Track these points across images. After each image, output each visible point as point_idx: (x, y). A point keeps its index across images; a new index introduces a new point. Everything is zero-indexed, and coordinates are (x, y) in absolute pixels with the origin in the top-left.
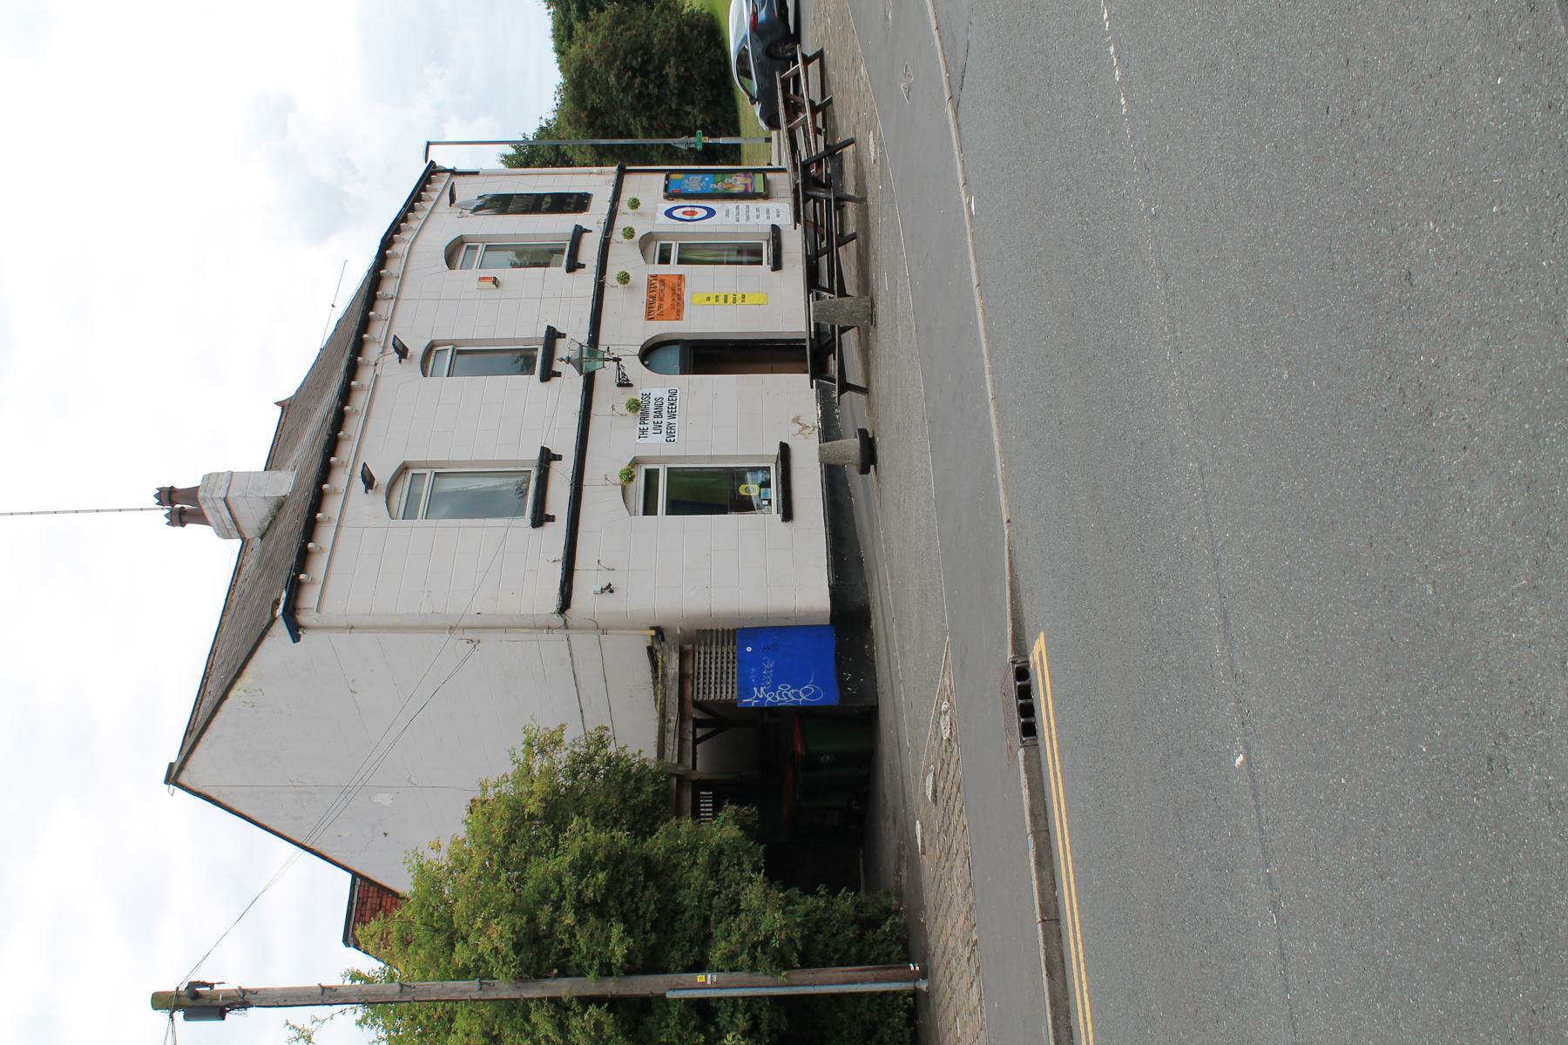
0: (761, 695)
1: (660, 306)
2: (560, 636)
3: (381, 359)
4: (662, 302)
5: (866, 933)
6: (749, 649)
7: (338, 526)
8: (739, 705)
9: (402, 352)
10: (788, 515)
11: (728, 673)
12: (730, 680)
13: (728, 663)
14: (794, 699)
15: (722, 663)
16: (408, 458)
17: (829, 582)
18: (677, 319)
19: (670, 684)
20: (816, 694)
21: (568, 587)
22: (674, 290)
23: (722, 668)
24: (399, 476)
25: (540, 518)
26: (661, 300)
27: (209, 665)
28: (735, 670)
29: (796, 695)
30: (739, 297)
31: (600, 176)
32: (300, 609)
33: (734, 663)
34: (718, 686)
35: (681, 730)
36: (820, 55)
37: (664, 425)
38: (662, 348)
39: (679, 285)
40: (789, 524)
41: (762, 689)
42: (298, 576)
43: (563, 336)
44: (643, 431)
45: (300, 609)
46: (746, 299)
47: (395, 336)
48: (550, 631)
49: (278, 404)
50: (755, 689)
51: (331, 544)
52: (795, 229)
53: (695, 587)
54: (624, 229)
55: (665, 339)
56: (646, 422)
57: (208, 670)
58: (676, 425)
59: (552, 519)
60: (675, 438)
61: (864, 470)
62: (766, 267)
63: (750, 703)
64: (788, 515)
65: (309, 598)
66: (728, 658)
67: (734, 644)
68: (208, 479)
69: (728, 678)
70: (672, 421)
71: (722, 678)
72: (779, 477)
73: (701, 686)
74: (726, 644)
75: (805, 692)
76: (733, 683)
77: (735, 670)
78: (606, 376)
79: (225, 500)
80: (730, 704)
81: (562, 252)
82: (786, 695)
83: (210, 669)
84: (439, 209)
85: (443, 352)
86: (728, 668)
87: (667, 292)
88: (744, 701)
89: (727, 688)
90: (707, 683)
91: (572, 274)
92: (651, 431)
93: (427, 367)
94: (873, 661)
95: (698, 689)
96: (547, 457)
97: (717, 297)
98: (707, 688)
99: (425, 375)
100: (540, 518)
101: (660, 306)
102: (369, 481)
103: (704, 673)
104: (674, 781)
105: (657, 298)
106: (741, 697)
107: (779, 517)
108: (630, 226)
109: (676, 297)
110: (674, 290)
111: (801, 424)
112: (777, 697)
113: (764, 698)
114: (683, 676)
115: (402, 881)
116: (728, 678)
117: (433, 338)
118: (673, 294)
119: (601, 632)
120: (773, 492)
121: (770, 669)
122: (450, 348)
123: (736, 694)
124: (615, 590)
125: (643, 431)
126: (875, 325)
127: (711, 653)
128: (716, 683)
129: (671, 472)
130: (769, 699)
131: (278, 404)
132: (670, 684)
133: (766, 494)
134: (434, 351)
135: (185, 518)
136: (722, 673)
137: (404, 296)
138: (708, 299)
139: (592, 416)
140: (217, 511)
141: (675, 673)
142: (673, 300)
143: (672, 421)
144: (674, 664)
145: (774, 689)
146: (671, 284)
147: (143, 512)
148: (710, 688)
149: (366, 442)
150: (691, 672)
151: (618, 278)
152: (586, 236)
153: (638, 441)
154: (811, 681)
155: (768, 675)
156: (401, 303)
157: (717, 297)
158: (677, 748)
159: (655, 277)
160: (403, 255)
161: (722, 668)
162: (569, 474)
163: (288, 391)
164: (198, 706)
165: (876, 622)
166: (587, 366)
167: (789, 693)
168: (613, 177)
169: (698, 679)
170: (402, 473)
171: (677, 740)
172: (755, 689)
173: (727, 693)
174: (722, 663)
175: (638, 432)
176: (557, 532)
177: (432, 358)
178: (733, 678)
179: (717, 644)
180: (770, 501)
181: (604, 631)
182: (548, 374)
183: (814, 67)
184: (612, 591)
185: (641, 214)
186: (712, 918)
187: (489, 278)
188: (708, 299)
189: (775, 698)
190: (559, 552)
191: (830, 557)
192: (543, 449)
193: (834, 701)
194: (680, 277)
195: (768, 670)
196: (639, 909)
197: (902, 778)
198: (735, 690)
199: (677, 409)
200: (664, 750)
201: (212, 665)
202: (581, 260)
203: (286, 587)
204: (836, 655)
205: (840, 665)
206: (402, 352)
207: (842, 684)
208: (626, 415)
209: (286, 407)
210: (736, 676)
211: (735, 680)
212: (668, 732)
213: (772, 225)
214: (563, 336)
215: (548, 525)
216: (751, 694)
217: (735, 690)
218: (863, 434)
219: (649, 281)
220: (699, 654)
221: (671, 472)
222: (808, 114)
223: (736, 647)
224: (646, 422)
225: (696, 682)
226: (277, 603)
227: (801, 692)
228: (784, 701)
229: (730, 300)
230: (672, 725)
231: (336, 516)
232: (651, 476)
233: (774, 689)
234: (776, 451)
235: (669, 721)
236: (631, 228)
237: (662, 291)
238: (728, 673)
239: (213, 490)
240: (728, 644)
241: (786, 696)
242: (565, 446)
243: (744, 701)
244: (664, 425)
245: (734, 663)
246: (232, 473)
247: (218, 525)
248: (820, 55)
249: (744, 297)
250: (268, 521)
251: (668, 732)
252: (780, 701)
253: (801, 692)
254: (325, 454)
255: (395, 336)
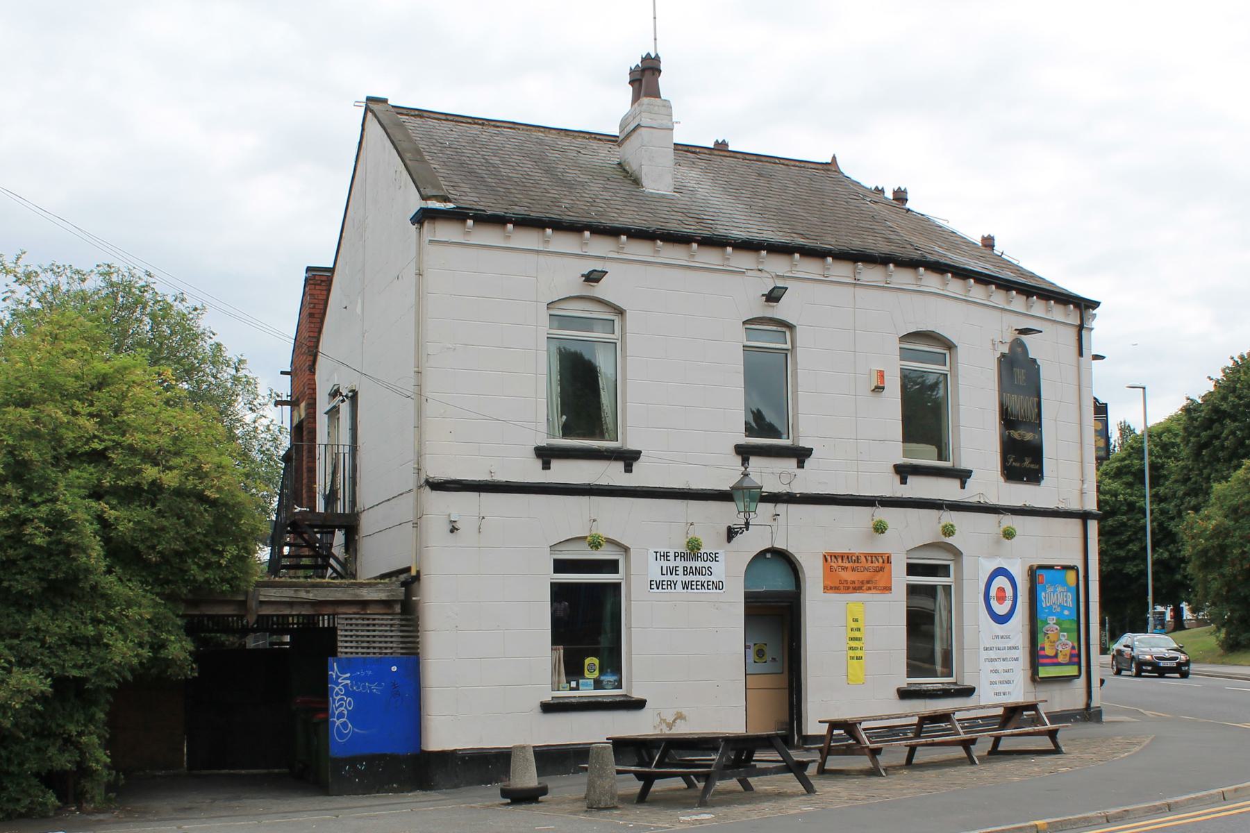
0: (340, 680)
1: (844, 568)
2: (411, 483)
3: (767, 275)
4: (850, 569)
5: (37, 780)
6: (394, 669)
7: (538, 252)
8: (330, 659)
9: (773, 297)
10: (548, 708)
11: (368, 648)
12: (360, 650)
13: (380, 648)
14: (337, 713)
15: (380, 642)
16: (628, 314)
17: (460, 750)
18: (825, 588)
19: (350, 592)
20: (341, 735)
21: (455, 488)
22: (868, 582)
23: (374, 642)
24: (610, 306)
25: (546, 455)
26: (853, 569)
27: (498, 124)
28: (371, 655)
29: (341, 715)
30: (859, 653)
31: (1078, 492)
32: (434, 223)
33: (380, 653)
34: (354, 638)
35: (303, 603)
36: (1057, 751)
37: (674, 578)
38: (790, 569)
39: (875, 588)
40: (539, 709)
41: (348, 682)
42: (470, 218)
43: (801, 465)
44: (665, 556)
45: (434, 223)
46: (855, 661)
47: (786, 288)
48: (416, 471)
49: (834, 158)
50: (348, 675)
51: (529, 248)
52: (820, 722)
53: (457, 615)
54: (952, 526)
55: (800, 575)
56: (678, 559)
57: (493, 123)
58: (673, 590)
59: (546, 466)
60: (656, 590)
61: (505, 793)
62: (904, 682)
63: (333, 670)
64: (548, 708)
65: (446, 231)
66: (386, 648)
67: (402, 654)
68: (664, 106)
69: (363, 648)
70: (679, 585)
71: (363, 642)
72: (600, 699)
73: (354, 621)
74: (401, 646)
75: (345, 725)
76: (357, 653)
77: (371, 655)
78: (728, 514)
79: (638, 126)
80: (333, 652)
81: (940, 458)
82: (341, 705)
83: (494, 126)
84: (1008, 317)
85: (783, 339)
86: (374, 648)
87: (865, 576)
88: (335, 664)
89: (352, 647)
90: (357, 628)
91: (892, 470)
92: (665, 564)
93: (762, 324)
94: (378, 792)
95: (351, 619)
96: (629, 458)
97: (859, 630)
98: (351, 628)
99: (744, 323)
100: (903, 472)
101: (844, 568)
102: (592, 278)
103: (368, 625)
104: (242, 598)
105: (856, 564)
106: (340, 662)
107: (904, 685)
108: (956, 532)
109: (857, 585)
110: (868, 582)
111: (674, 721)
112: (339, 697)
113: (338, 684)
114: (364, 604)
115: (998, 249)
116: (363, 648)
117: (797, 326)
118: (862, 582)
119: (415, 521)
120: (587, 692)
121: (371, 690)
122: (789, 346)
123: (344, 656)
124: (454, 534)
125: (665, 556)
126: (586, 811)
127: (392, 631)
128: (357, 636)
129: (617, 587)
130: (337, 689)
131: (834, 158)
132: (350, 592)
133: (586, 685)
134: (784, 329)
135: (637, 84)
136: (368, 642)
137: (859, 291)
138: (855, 620)
139: (686, 501)
140: (634, 118)
141: (362, 596)
142: (854, 582)
143: (679, 585)
144: (372, 594)
145: (348, 694)
146: (877, 578)
147: (657, 37)
148: (351, 630)
149: (650, 268)
150: (368, 612)
151: (881, 522)
152: (956, 483)
153: (652, 551)
154: (356, 730)
155: (364, 687)
156: (851, 289)
157: (859, 630)
158: (278, 599)
159: (888, 560)
160: (920, 286)
161: (374, 642)
162: (604, 481)
163: (845, 167)
164: (451, 118)
165: (419, 795)
166: (737, 495)
167: (343, 708)
168: (1074, 506)
169: (363, 619)
170: (615, 309)
171: (287, 599)
172: (348, 675)
173: (345, 647)
174: (380, 642)
175: (663, 550)
176: (534, 473)
177: (774, 328)
178: (363, 653)
179: (402, 637)
180: (577, 688)
181: (416, 525)
182: (744, 453)
183: (1046, 743)
184: (452, 531)
185: (998, 542)
186: (16, 642)
187: (882, 381)
188: (855, 620)
189: (337, 694)
190: (502, 477)
191: (493, 751)
192: (639, 452)
193: (334, 752)
194: (888, 589)
195: (370, 687)
196: (21, 575)
197: (196, 819)
198: (349, 655)
199: (696, 591)
200: (271, 587)
201: (498, 127)
202: (910, 479)
203: (458, 208)
204: (385, 755)
205: (372, 759)
206: (773, 297)
207: (353, 761)
208: (939, 523)
209: (829, 167)
210: (364, 656)
211: (360, 655)
212: (296, 591)
213: (975, 688)
214: (801, 465)
215: (539, 463)
216: (343, 671)
217: (349, 655)
218: (543, 791)
219: (881, 555)
220: (391, 620)
221: (617, 587)
222: (963, 736)
223: (399, 656)
224: (678, 559)
225: (358, 616)
226: (446, 199)
227: (344, 720)
228: (334, 702)
229: (854, 644)
230: (303, 594)
231: (551, 249)
232: (612, 566)
233: (348, 694)
234: (636, 695)
235: (308, 592)
236: (953, 533)
237: (867, 569)
238: (368, 648)
239: (650, 112)
240: (402, 648)
241: (340, 705)
242: (641, 476)
243: (335, 664)
244: (674, 578)
245: (380, 653)
246: (672, 129)
247: (627, 119)
248: (1057, 751)
249: (859, 658)
250: (628, 170)
251: (296, 591)
252: (334, 700)
253: (344, 720)
254: (629, 229)
255: (786, 288)
